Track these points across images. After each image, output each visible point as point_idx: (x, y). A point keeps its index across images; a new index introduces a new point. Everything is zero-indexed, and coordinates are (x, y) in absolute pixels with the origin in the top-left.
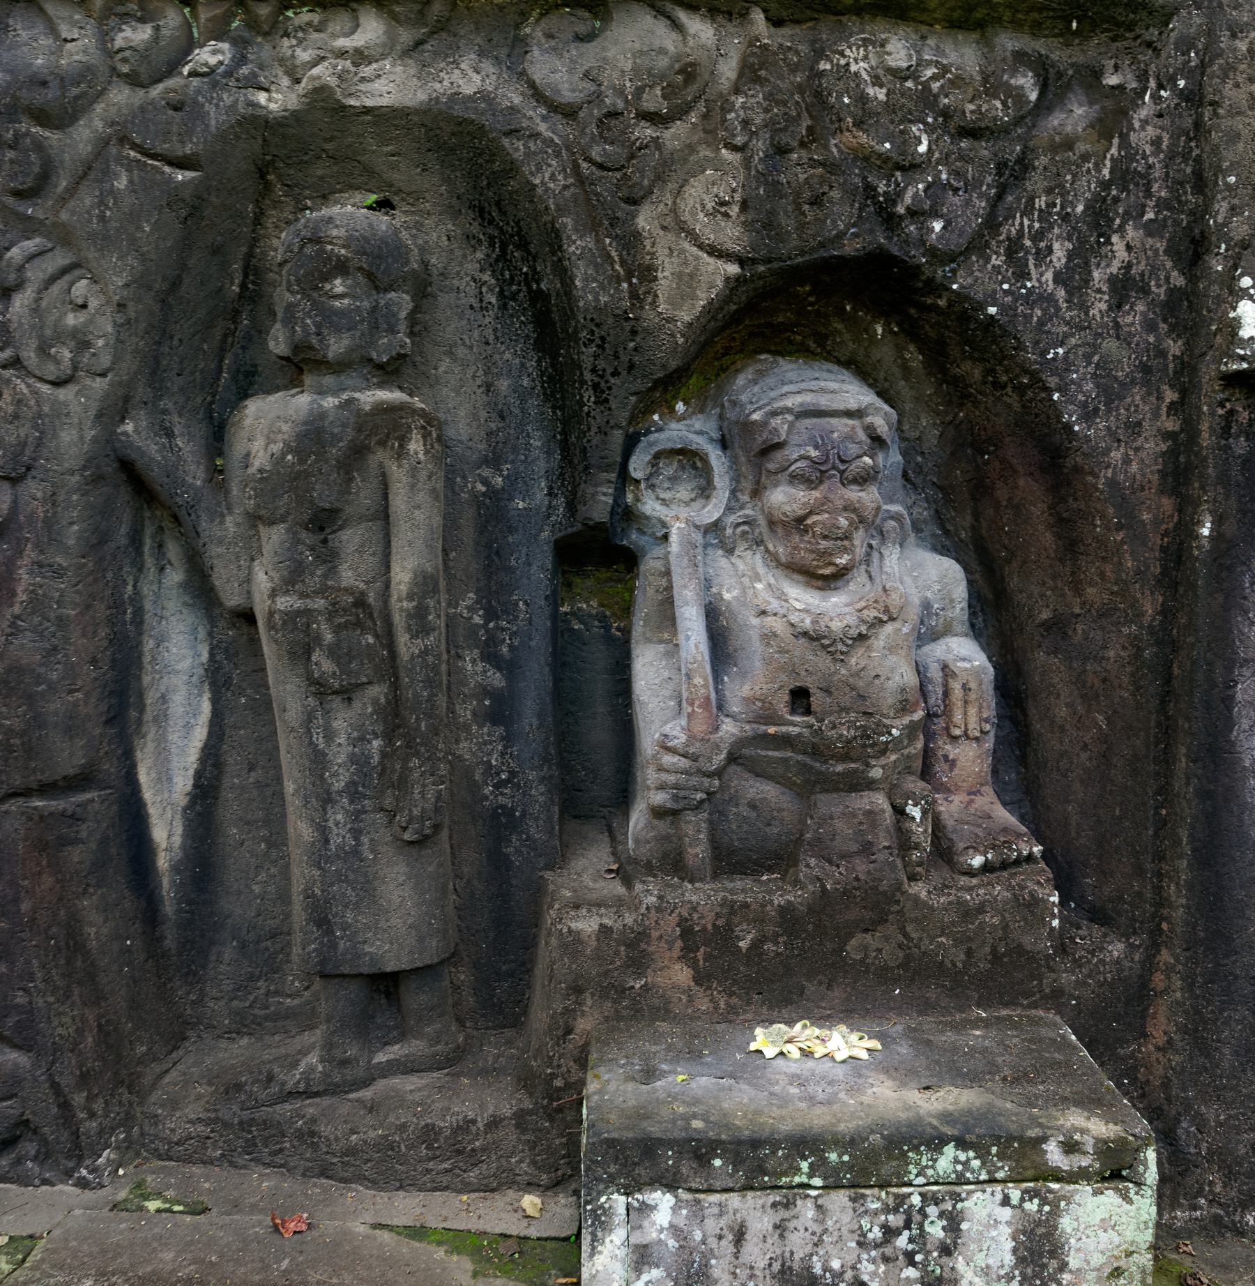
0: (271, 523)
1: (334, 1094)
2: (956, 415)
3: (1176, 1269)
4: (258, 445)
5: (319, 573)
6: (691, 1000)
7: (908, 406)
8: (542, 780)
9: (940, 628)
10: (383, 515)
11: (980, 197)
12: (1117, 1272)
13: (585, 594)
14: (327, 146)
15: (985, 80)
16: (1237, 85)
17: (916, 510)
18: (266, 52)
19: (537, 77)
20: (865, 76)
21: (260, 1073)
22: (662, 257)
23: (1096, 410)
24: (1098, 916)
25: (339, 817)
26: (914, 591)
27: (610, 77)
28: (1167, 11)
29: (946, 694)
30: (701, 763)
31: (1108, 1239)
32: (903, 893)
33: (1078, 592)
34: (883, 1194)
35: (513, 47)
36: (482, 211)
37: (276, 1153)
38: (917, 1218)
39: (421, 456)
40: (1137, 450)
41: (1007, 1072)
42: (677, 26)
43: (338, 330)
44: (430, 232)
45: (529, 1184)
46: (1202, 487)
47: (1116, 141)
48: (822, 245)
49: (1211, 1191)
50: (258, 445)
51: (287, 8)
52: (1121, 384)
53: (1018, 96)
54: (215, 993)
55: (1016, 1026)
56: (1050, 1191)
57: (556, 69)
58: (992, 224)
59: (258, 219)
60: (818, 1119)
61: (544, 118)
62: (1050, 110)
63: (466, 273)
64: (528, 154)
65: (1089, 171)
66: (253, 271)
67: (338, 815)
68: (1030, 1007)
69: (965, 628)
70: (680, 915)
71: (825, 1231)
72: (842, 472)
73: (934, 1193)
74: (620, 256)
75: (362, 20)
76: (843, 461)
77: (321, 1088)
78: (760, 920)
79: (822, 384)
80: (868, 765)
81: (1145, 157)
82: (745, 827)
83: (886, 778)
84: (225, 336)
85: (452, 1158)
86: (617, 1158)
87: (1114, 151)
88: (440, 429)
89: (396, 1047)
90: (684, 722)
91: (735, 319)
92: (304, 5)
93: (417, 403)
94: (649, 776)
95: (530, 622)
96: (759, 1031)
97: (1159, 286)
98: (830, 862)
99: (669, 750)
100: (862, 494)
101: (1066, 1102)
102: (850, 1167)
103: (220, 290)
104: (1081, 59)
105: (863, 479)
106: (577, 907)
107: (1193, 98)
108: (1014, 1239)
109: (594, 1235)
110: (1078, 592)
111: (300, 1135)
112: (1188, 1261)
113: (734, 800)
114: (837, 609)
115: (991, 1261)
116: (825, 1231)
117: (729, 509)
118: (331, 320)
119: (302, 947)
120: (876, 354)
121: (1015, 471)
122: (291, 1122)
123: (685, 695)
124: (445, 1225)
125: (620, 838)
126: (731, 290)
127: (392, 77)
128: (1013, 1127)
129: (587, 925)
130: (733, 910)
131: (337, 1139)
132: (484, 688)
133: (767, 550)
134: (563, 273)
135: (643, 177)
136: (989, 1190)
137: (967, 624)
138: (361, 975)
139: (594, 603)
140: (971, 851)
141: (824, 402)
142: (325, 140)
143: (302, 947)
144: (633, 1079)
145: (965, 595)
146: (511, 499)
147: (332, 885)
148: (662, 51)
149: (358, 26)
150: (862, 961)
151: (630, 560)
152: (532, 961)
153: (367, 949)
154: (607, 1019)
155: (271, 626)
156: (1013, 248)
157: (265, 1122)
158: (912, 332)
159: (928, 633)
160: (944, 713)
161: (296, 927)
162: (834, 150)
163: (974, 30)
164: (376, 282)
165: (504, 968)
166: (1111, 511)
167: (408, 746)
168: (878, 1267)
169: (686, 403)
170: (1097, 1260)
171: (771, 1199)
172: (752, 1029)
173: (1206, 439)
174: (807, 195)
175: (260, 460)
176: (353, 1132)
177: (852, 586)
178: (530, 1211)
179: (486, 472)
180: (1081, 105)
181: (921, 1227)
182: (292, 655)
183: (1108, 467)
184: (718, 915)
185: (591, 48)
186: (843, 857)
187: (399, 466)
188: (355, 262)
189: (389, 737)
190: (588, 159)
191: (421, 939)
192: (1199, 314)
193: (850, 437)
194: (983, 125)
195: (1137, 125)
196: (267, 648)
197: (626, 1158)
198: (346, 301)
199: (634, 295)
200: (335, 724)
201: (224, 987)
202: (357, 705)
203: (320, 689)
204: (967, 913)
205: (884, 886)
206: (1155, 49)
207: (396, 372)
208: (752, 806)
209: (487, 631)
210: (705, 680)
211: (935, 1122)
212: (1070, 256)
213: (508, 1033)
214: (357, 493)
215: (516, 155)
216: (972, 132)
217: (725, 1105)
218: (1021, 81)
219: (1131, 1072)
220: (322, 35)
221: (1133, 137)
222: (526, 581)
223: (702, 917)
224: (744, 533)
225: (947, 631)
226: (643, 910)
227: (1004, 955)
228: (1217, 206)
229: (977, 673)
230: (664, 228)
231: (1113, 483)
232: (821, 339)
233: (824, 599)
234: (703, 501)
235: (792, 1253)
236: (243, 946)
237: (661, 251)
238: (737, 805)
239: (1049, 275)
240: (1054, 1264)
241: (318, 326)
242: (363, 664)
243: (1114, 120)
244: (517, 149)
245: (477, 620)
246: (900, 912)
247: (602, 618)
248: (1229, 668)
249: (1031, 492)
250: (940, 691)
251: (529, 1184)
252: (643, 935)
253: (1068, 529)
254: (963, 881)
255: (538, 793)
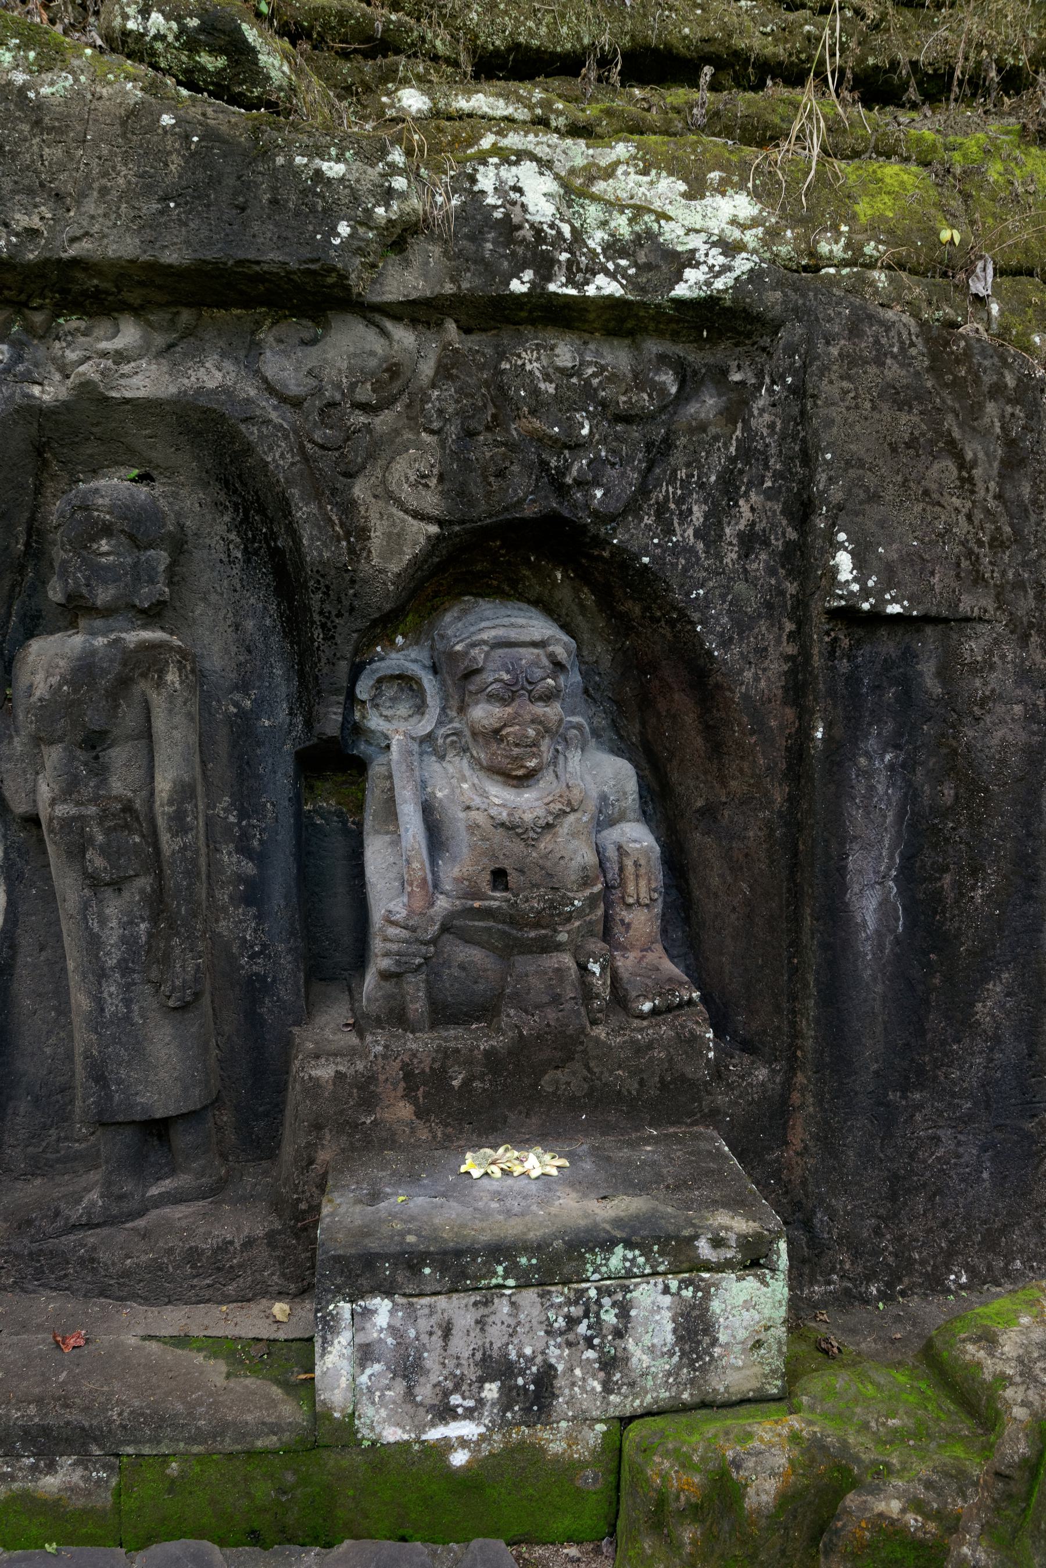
0: (51, 743)
1: (112, 1224)
2: (624, 643)
3: (812, 1336)
4: (39, 678)
5: (92, 784)
6: (413, 1131)
7: (586, 636)
8: (290, 951)
9: (616, 815)
10: (147, 734)
11: (633, 470)
12: (758, 1344)
13: (325, 794)
14: (94, 430)
15: (636, 377)
16: (831, 382)
17: (595, 720)
18: (41, 353)
19: (269, 374)
20: (537, 373)
21: (49, 1209)
22: (374, 521)
23: (731, 639)
24: (748, 1046)
25: (113, 989)
26: (593, 786)
27: (329, 374)
28: (776, 323)
29: (621, 869)
30: (419, 933)
31: (749, 1317)
32: (586, 1035)
33: (724, 784)
34: (566, 1290)
35: (250, 349)
36: (227, 483)
37: (60, 1279)
38: (594, 1308)
39: (177, 685)
40: (764, 670)
41: (670, 1181)
42: (384, 333)
43: (105, 582)
44: (184, 500)
45: (280, 1293)
46: (815, 700)
47: (740, 425)
48: (506, 509)
49: (841, 1268)
50: (39, 678)
51: (59, 317)
52: (750, 617)
53: (662, 390)
54: (12, 1141)
55: (680, 1141)
56: (702, 1280)
57: (284, 367)
58: (644, 491)
59: (38, 490)
60: (512, 1229)
61: (275, 408)
62: (688, 400)
63: (215, 534)
64: (261, 437)
65: (719, 449)
66: (36, 532)
67: (111, 988)
68: (692, 1124)
69: (637, 814)
70: (402, 1061)
71: (519, 1323)
72: (530, 692)
73: (608, 1286)
74: (340, 519)
75: (121, 327)
76: (530, 683)
77: (101, 1220)
78: (469, 1062)
79: (513, 620)
80: (555, 931)
81: (762, 438)
82: (457, 985)
83: (571, 941)
84: (13, 586)
85: (214, 1275)
86: (342, 1271)
87: (738, 433)
88: (194, 662)
89: (167, 1181)
90: (405, 900)
91: (439, 569)
92: (73, 314)
93: (175, 641)
94: (377, 945)
95: (276, 819)
96: (469, 1155)
97: (777, 540)
98: (526, 1012)
99: (393, 923)
100: (547, 709)
101: (715, 1204)
102: (537, 1269)
103: (7, 548)
104: (711, 360)
105: (547, 697)
106: (317, 1057)
107: (798, 392)
108: (674, 1321)
109: (324, 1338)
110: (724, 784)
111: (82, 1261)
112: (823, 1328)
113: (447, 963)
114: (527, 803)
115: (655, 1341)
116: (519, 1323)
117: (440, 723)
118: (98, 573)
119: (84, 1101)
120: (558, 595)
121: (671, 688)
122: (74, 1250)
123: (406, 877)
124: (206, 1333)
125: (357, 996)
126: (433, 546)
127: (148, 374)
128: (671, 1228)
129: (325, 1072)
130: (446, 1054)
131: (114, 1264)
132: (239, 876)
133: (472, 756)
134: (293, 533)
135: (357, 456)
136: (652, 1281)
137: (639, 812)
138: (133, 1122)
139: (333, 802)
140: (641, 999)
141: (513, 635)
142: (93, 425)
143: (84, 1101)
144: (361, 1202)
145: (636, 788)
146: (258, 719)
147: (107, 1047)
148: (372, 353)
149: (118, 331)
150: (554, 1093)
151: (361, 766)
152: (284, 1102)
153: (139, 1099)
154: (343, 1150)
155: (51, 831)
156: (661, 510)
157: (51, 1252)
158: (584, 577)
159: (606, 818)
160: (620, 885)
161: (78, 1083)
162: (514, 433)
163: (626, 337)
164: (137, 542)
165: (261, 1109)
166: (745, 719)
167: (171, 928)
168: (563, 1352)
169: (404, 636)
170: (742, 1334)
171: (473, 1299)
172: (464, 1154)
173: (817, 661)
174: (492, 469)
175: (41, 690)
176: (128, 1256)
177: (542, 784)
178: (280, 1317)
179: (237, 696)
180: (711, 397)
181: (597, 1315)
182: (69, 853)
183: (742, 684)
184: (434, 1060)
185: (313, 350)
186: (537, 1007)
187: (159, 694)
188: (118, 526)
189: (154, 920)
190: (312, 441)
191: (186, 1089)
192: (809, 562)
193: (536, 663)
194: (633, 413)
195: (756, 412)
196: (50, 849)
197: (350, 1271)
198: (111, 558)
199: (351, 550)
200: (107, 911)
201: (20, 1137)
202: (126, 894)
203: (94, 882)
204: (639, 1049)
205: (571, 1030)
206: (768, 353)
207: (159, 615)
208: (462, 967)
209: (240, 828)
210: (422, 864)
211: (608, 1227)
212: (706, 517)
213: (265, 1164)
214: (123, 717)
215: (251, 438)
216: (626, 419)
217: (436, 1221)
218: (663, 378)
219: (776, 1174)
220: (88, 339)
221: (753, 422)
222: (272, 786)
223: (421, 1062)
224: (453, 742)
225: (622, 818)
226: (371, 1058)
227: (670, 1083)
228: (818, 477)
229: (646, 852)
230: (375, 496)
231: (746, 697)
232: (514, 583)
233: (518, 795)
234: (418, 717)
235: (491, 1344)
236: (36, 1100)
237: (374, 516)
238: (449, 967)
239: (690, 532)
240: (707, 1340)
241: (88, 579)
242: (130, 860)
243: (737, 408)
244: (252, 433)
245: (232, 819)
246: (585, 1052)
247: (340, 814)
248: (842, 844)
249: (683, 702)
250: (616, 868)
251: (280, 1293)
252: (372, 1079)
253: (713, 733)
254: (636, 1023)
255: (286, 961)
